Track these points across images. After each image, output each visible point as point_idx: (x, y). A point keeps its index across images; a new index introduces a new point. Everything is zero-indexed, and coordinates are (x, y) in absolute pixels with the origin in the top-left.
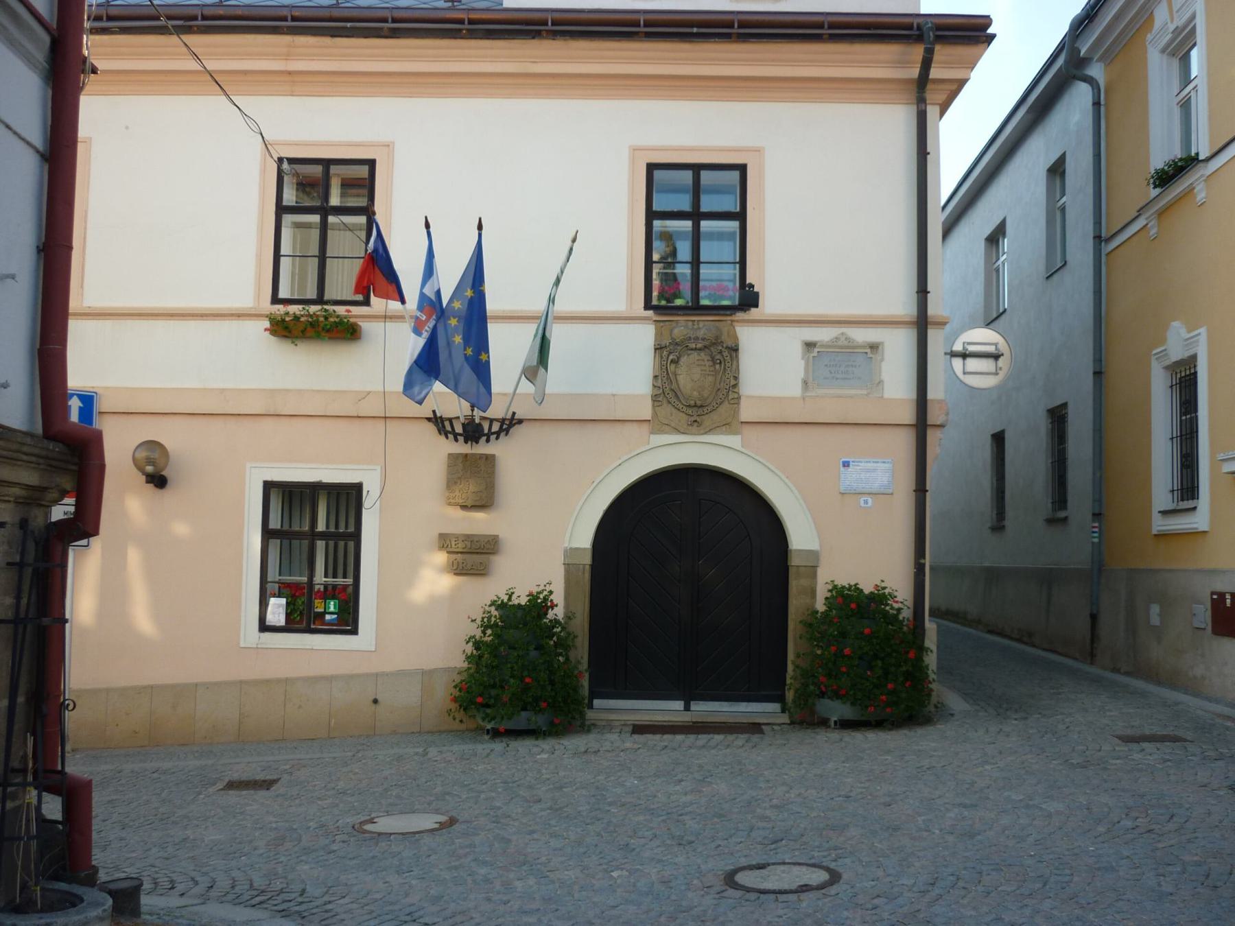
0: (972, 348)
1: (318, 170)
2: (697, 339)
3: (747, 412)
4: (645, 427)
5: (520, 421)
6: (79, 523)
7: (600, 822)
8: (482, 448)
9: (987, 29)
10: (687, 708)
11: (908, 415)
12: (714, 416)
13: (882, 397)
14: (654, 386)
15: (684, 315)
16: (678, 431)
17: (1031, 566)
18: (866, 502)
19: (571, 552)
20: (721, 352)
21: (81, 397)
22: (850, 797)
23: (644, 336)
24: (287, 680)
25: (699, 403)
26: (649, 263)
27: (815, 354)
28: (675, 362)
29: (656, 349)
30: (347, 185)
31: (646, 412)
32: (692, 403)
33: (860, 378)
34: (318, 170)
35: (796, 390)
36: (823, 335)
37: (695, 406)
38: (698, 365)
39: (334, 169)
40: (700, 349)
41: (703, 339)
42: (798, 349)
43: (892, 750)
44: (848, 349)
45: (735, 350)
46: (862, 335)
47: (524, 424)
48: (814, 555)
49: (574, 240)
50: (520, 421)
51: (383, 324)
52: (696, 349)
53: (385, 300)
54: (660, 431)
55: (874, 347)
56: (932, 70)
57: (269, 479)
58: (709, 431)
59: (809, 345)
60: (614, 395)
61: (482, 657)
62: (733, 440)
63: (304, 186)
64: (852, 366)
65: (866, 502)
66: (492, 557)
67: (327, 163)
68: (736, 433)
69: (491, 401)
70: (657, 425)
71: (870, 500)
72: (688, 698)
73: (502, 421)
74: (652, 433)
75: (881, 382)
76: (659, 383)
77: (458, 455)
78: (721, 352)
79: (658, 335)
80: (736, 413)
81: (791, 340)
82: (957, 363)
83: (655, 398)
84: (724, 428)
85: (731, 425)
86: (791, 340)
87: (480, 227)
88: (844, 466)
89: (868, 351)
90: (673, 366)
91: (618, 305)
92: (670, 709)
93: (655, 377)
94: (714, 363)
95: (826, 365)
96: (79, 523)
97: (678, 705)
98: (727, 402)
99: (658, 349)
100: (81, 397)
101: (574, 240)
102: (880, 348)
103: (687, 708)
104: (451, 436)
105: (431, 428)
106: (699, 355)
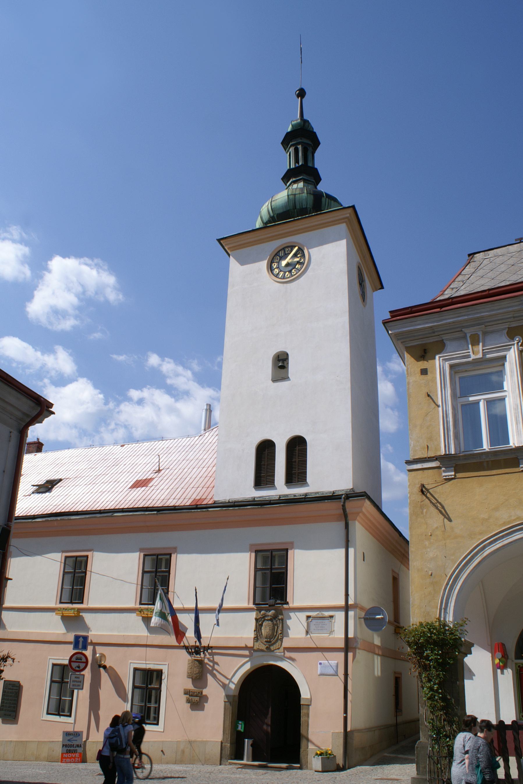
9: (379, 646)
17: (410, 592)
33: (326, 629)
38: (268, 626)
41: (271, 616)
42: (305, 618)
43: (464, 630)
49: (228, 579)
51: (11, 546)
55: (331, 617)
59: (308, 617)
64: (324, 624)
69: (509, 768)
81: (302, 616)
88: (320, 664)
91: (245, 605)
95: (314, 624)
101: (228, 579)
102: (334, 617)
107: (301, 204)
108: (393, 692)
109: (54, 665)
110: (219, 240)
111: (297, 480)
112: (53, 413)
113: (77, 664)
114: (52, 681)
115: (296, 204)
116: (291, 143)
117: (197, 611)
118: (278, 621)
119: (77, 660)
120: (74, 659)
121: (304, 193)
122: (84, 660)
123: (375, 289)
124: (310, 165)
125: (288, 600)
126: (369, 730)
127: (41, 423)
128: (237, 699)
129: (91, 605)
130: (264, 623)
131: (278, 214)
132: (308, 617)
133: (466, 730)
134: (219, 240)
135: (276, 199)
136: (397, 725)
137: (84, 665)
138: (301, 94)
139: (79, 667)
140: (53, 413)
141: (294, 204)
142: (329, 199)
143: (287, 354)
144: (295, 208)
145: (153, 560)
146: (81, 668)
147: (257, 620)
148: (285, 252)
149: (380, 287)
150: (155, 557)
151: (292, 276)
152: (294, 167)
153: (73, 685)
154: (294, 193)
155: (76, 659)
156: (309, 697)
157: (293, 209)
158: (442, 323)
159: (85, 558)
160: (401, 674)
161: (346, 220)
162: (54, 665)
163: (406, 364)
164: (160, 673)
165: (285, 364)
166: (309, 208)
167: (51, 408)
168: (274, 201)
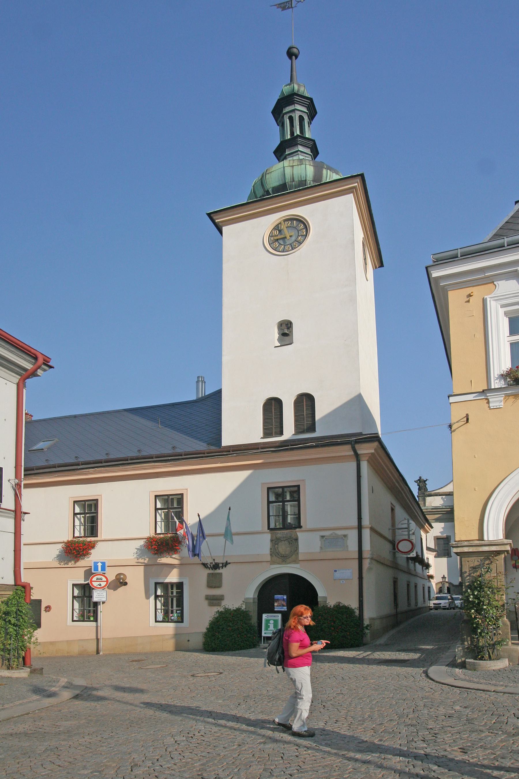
1: (281, 490)
2: (284, 537)
3: (301, 557)
5: (230, 563)
6: (487, 761)
7: (371, 728)
8: (218, 571)
12: (290, 559)
13: (348, 551)
14: (271, 552)
15: (279, 531)
16: (279, 564)
18: (343, 582)
20: (292, 541)
21: (101, 562)
23: (268, 537)
24: (163, 635)
26: (269, 516)
27: (325, 539)
29: (271, 541)
30: (291, 493)
31: (269, 558)
32: (283, 556)
34: (280, 490)
35: (318, 550)
36: (326, 533)
37: (284, 556)
39: (285, 489)
40: (285, 540)
42: (318, 538)
46: (340, 533)
47: (231, 564)
48: (325, 598)
50: (230, 563)
52: (283, 540)
54: (273, 564)
55: (345, 536)
57: (156, 582)
58: (289, 563)
59: (323, 537)
60: (258, 555)
62: (297, 566)
63: (277, 495)
65: (343, 582)
67: (283, 488)
68: (298, 563)
70: (272, 562)
71: (344, 581)
73: (223, 564)
74: (271, 564)
75: (347, 546)
76: (272, 551)
77: (211, 573)
78: (292, 541)
80: (297, 557)
83: (271, 555)
84: (294, 562)
85: (296, 561)
87: (230, 509)
88: (335, 571)
89: (343, 537)
90: (276, 546)
91: (260, 529)
93: (271, 549)
94: (290, 544)
96: (487, 761)
98: (294, 555)
99: (272, 541)
104: (211, 569)
105: (202, 566)
106: (284, 542)
107: (300, 176)
108: (392, 591)
113: (99, 583)
114: (74, 597)
115: (294, 176)
117: (292, 8)
119: (98, 580)
125: (301, 525)
126: (381, 618)
128: (256, 601)
129: (103, 538)
131: (273, 187)
133: (33, 601)
134: (209, 215)
135: (270, 172)
139: (100, 585)
141: (292, 176)
142: (330, 171)
144: (293, 181)
146: (102, 586)
152: (289, 137)
155: (97, 579)
157: (291, 182)
159: (95, 502)
160: (397, 579)
163: (140, 686)
166: (309, 180)
168: (268, 173)
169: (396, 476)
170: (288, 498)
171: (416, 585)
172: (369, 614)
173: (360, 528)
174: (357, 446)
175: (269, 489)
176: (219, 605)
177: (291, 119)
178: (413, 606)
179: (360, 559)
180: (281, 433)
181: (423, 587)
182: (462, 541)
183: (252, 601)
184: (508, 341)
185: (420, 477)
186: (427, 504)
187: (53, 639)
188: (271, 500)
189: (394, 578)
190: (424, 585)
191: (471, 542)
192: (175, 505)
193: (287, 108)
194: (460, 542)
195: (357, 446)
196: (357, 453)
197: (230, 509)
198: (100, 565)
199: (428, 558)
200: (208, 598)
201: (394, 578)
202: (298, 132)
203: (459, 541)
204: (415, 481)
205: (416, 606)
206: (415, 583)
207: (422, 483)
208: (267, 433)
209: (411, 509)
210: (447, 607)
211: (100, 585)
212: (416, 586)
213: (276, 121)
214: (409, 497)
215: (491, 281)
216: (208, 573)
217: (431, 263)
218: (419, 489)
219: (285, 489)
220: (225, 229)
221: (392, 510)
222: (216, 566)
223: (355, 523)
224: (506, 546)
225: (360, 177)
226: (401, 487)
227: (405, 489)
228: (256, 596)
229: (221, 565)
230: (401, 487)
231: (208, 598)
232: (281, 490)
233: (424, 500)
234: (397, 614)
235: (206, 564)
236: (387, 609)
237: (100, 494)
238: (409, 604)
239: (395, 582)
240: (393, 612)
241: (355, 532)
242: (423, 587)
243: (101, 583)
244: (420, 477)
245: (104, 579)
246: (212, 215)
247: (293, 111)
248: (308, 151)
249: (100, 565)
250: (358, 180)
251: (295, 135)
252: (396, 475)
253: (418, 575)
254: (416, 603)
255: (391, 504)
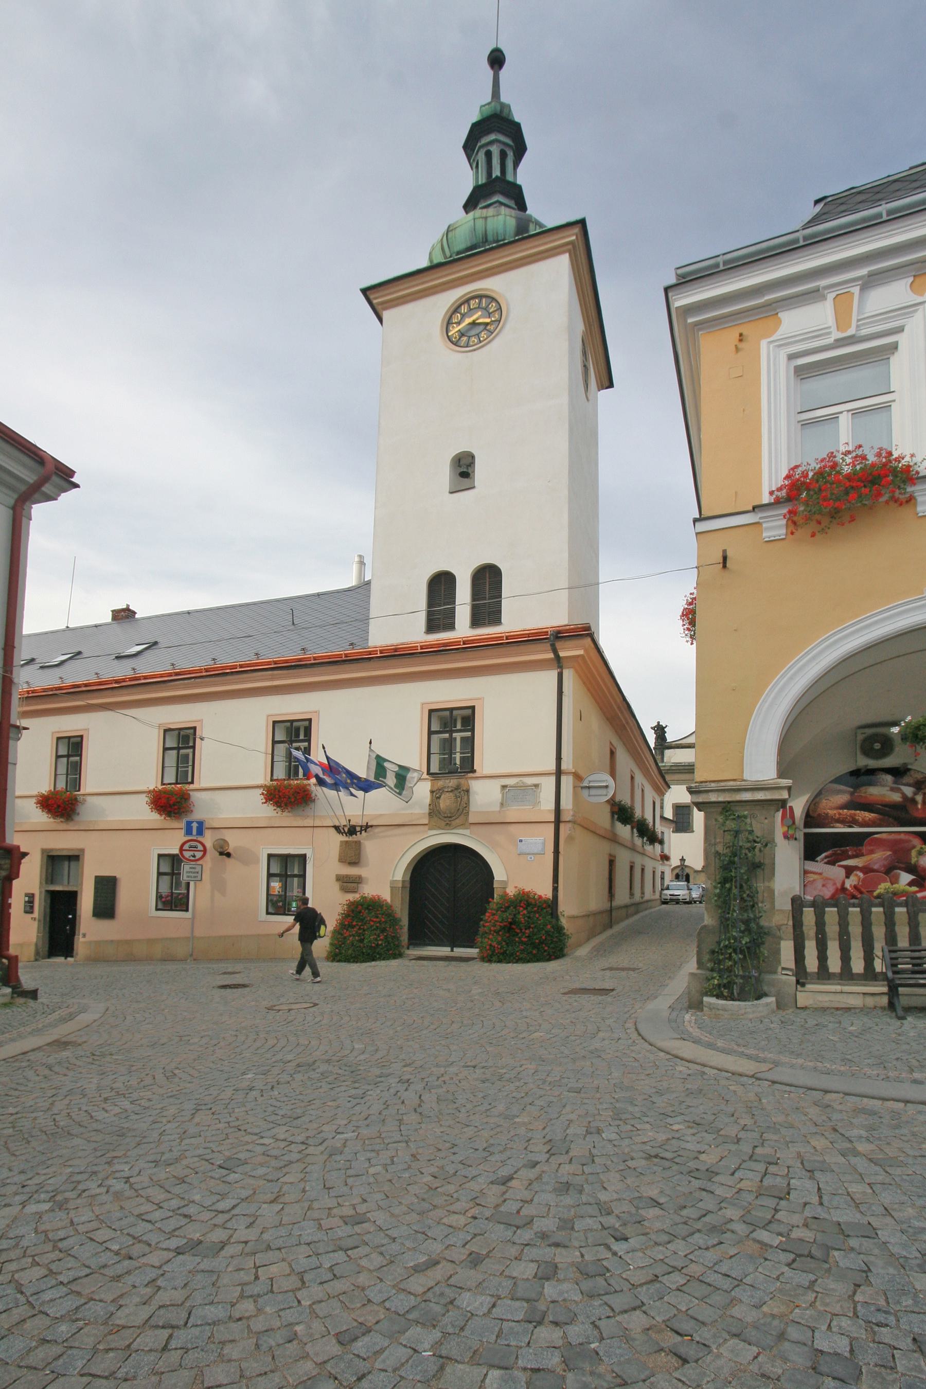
0: (591, 784)
1: (447, 713)
3: (472, 819)
4: (427, 827)
8: (354, 838)
10: (452, 950)
11: (552, 818)
12: (457, 821)
16: (440, 828)
19: (393, 882)
21: (198, 822)
22: (827, 1117)
25: (449, 815)
28: (439, 798)
42: (499, 789)
44: (524, 788)
45: (468, 791)
46: (530, 781)
48: (505, 883)
50: (371, 826)
53: (14, 668)
55: (536, 786)
56: (47, 485)
61: (880, 1140)
62: (467, 832)
66: (360, 885)
72: (453, 946)
73: (361, 827)
79: (432, 786)
80: (467, 819)
81: (496, 785)
82: (586, 792)
85: (465, 824)
86: (496, 785)
87: (370, 743)
92: (445, 951)
97: (449, 949)
100: (198, 822)
103: (452, 950)
109: (160, 856)
110: (365, 291)
111: (487, 621)
112: (76, 486)
113: (192, 853)
114: (160, 874)
116: (479, 144)
118: (462, 793)
120: (186, 847)
121: (500, 214)
122: (200, 847)
123: (601, 387)
124: (510, 178)
127: (56, 499)
128: (408, 885)
129: (204, 784)
130: (442, 797)
132: (504, 787)
134: (365, 291)
136: (611, 910)
137: (201, 854)
138: (497, 60)
139: (194, 856)
140: (76, 486)
143: (473, 457)
145: (287, 728)
146: (197, 858)
147: (432, 792)
148: (469, 305)
149: (607, 384)
150: (289, 724)
151: (480, 342)
153: (188, 877)
154: (484, 216)
156: (505, 879)
158: (757, 302)
159: (192, 731)
160: (615, 857)
161: (570, 247)
162: (160, 856)
164: (303, 858)
165: (470, 471)
167: (72, 477)
169: (618, 701)
170: (459, 727)
171: (612, 858)
172: (568, 908)
173: (559, 773)
174: (559, 645)
175: (431, 711)
176: (354, 891)
177: (489, 155)
178: (637, 897)
179: (558, 821)
180: (451, 626)
181: (654, 872)
182: (706, 782)
183: (400, 885)
184: (798, 422)
185: (659, 723)
186: (665, 759)
187: (129, 937)
188: (433, 729)
189: (610, 855)
190: (634, 863)
191: (722, 784)
192: (302, 737)
193: (485, 138)
194: (703, 784)
195: (559, 645)
196: (559, 655)
197: (370, 743)
198: (195, 825)
199: (663, 833)
200: (339, 878)
201: (610, 855)
202: (496, 172)
203: (702, 782)
204: (652, 728)
205: (642, 898)
206: (643, 865)
207: (660, 731)
208: (433, 625)
209: (642, 759)
210: (688, 900)
211: (194, 856)
212: (643, 870)
213: (469, 158)
214: (637, 735)
215: (770, 311)
216: (341, 842)
217: (673, 281)
218: (657, 739)
219: (455, 712)
220: (386, 315)
221: (612, 753)
222: (352, 831)
223: (552, 767)
224: (781, 791)
225: (580, 225)
226: (626, 719)
227: (630, 722)
228: (408, 878)
229: (358, 829)
230: (626, 719)
231: (339, 878)
232: (447, 713)
233: (662, 754)
234: (611, 910)
235: (338, 827)
236: (596, 901)
237: (199, 718)
238: (632, 894)
239: (612, 863)
240: (607, 906)
241: (553, 779)
242: (654, 872)
243: (196, 853)
244: (659, 723)
245: (200, 847)
246: (368, 293)
247: (491, 143)
248: (512, 203)
249: (195, 825)
250: (577, 230)
251: (494, 176)
252: (619, 699)
253: (647, 854)
254: (643, 893)
255: (632, 771)
